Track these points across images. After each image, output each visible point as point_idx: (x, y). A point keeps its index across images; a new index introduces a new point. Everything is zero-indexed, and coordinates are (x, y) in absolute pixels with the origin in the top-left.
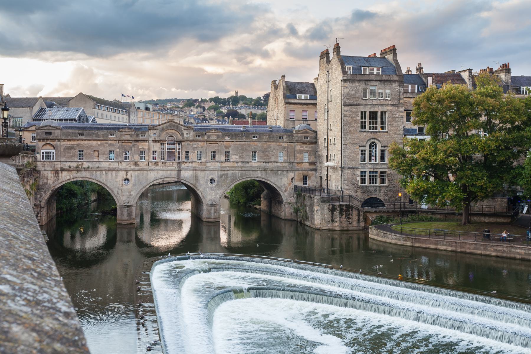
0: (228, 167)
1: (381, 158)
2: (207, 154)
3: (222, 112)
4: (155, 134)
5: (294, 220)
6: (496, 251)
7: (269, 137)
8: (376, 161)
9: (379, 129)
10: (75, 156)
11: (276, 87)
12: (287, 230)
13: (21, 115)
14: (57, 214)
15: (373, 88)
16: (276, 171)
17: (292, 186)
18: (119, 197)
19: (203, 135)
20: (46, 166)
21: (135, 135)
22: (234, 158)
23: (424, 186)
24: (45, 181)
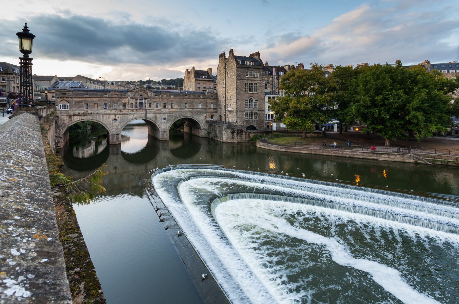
6: (335, 153)
7: (194, 96)
8: (252, 107)
10: (82, 107)
12: (204, 143)
13: (44, 85)
14: (69, 139)
16: (198, 113)
17: (205, 120)
19: (159, 95)
20: (63, 113)
22: (176, 107)
23: (295, 121)
24: (63, 122)
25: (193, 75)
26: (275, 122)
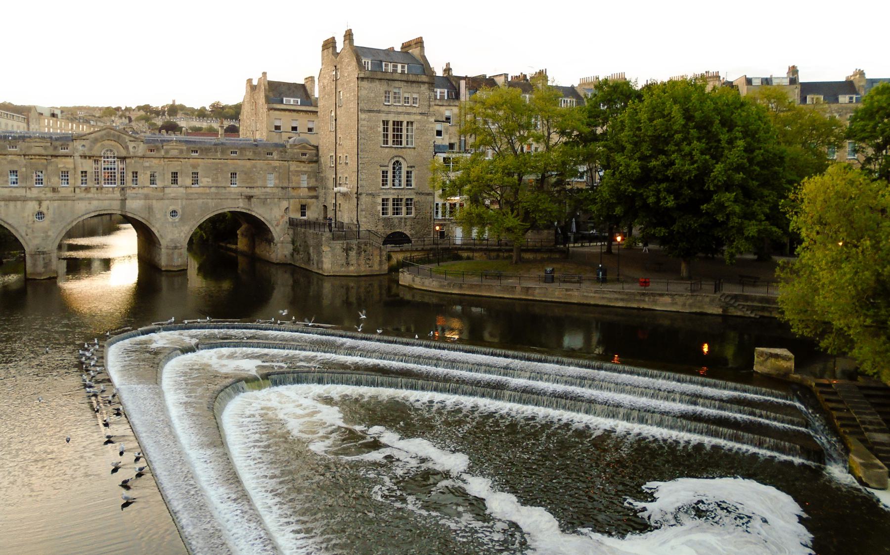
0: (197, 193)
1: (407, 181)
2: (166, 176)
3: (155, 124)
4: (83, 146)
5: (290, 264)
7: (254, 153)
8: (400, 185)
9: (404, 143)
11: (253, 88)
15: (397, 91)
17: (286, 219)
18: (30, 239)
19: (158, 149)
21: (52, 148)
22: (204, 181)
25: (262, 95)
26: (460, 223)
